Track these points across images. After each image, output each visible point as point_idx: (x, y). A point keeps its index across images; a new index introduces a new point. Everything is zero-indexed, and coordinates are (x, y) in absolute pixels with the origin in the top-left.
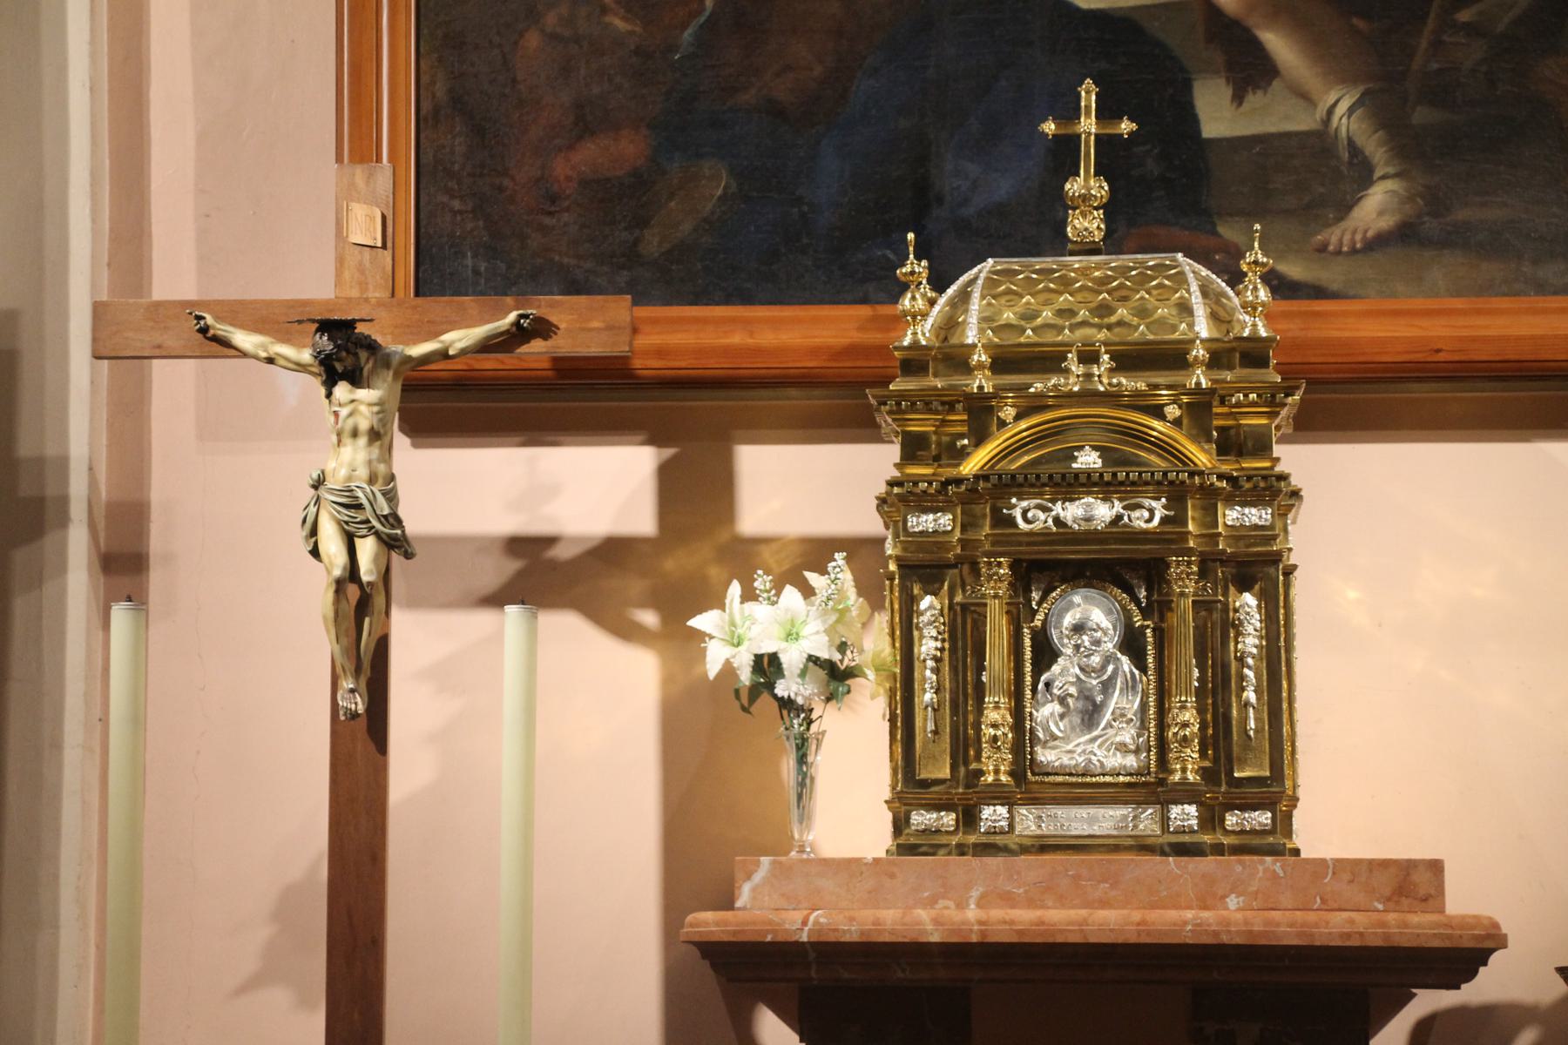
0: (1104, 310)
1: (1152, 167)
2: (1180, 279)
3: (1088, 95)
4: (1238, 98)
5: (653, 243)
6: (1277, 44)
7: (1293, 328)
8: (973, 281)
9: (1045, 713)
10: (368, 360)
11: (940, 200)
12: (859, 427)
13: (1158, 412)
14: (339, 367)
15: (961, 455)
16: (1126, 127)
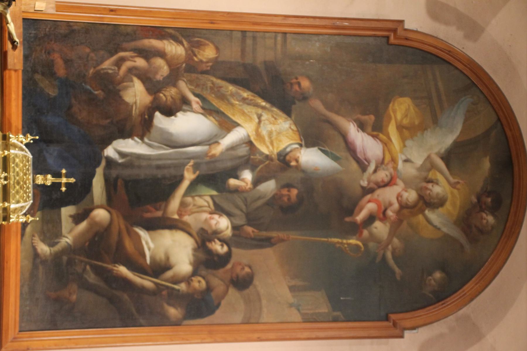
0: (18, 183)
1: (54, 196)
2: (25, 201)
3: (72, 180)
4: (71, 216)
5: (38, 77)
6: (83, 225)
7: (14, 229)
8: (26, 152)
10: (6, 4)
11: (48, 146)
16: (64, 189)
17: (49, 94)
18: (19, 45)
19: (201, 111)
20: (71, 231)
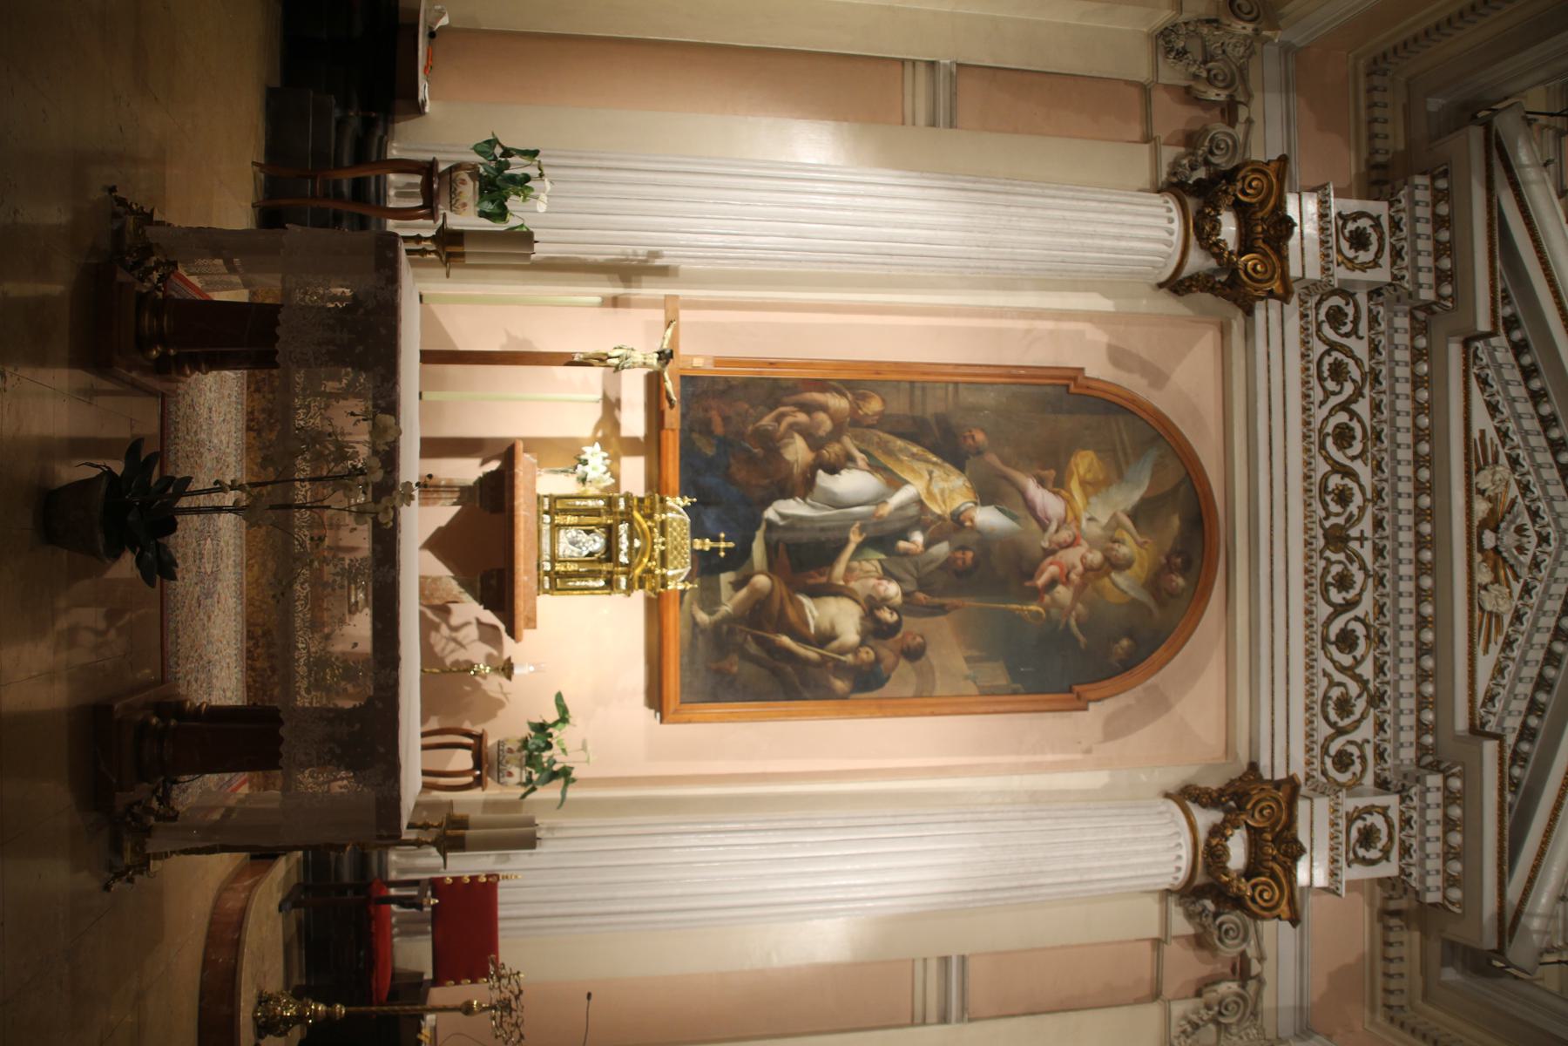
0: (676, 548)
2: (683, 567)
5: (695, 436)
6: (743, 592)
9: (572, 532)
13: (649, 561)
15: (639, 511)
16: (722, 554)
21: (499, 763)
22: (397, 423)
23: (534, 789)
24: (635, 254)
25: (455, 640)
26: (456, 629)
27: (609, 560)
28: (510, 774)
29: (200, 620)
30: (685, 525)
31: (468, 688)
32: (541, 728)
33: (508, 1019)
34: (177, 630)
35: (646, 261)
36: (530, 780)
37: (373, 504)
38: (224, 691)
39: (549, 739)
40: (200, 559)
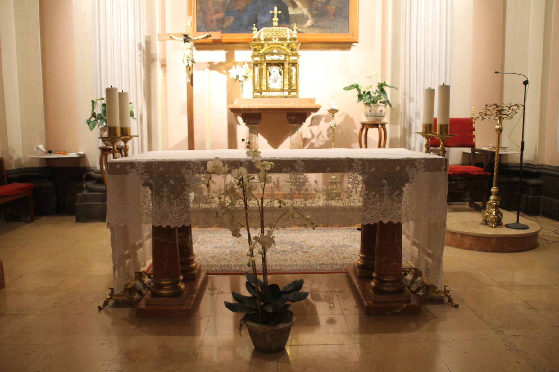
0: (277, 34)
2: (286, 30)
3: (276, 8)
4: (293, 9)
5: (224, 26)
6: (298, 3)
9: (270, 82)
11: (258, 21)
12: (249, 48)
13: (283, 45)
14: (186, 40)
15: (260, 51)
16: (280, 12)
17: (233, 21)
18: (209, 34)
19: (141, 290)
20: (301, 9)
21: (376, 116)
22: (212, 160)
23: (388, 101)
24: (140, 56)
25: (318, 136)
26: (313, 136)
27: (283, 64)
28: (381, 111)
29: (314, 251)
30: (266, 29)
31: (340, 131)
32: (360, 97)
33: (505, 111)
34: (320, 265)
35: (143, 51)
36: (384, 102)
37: (260, 173)
38: (344, 239)
39: (366, 93)
40: (285, 252)
